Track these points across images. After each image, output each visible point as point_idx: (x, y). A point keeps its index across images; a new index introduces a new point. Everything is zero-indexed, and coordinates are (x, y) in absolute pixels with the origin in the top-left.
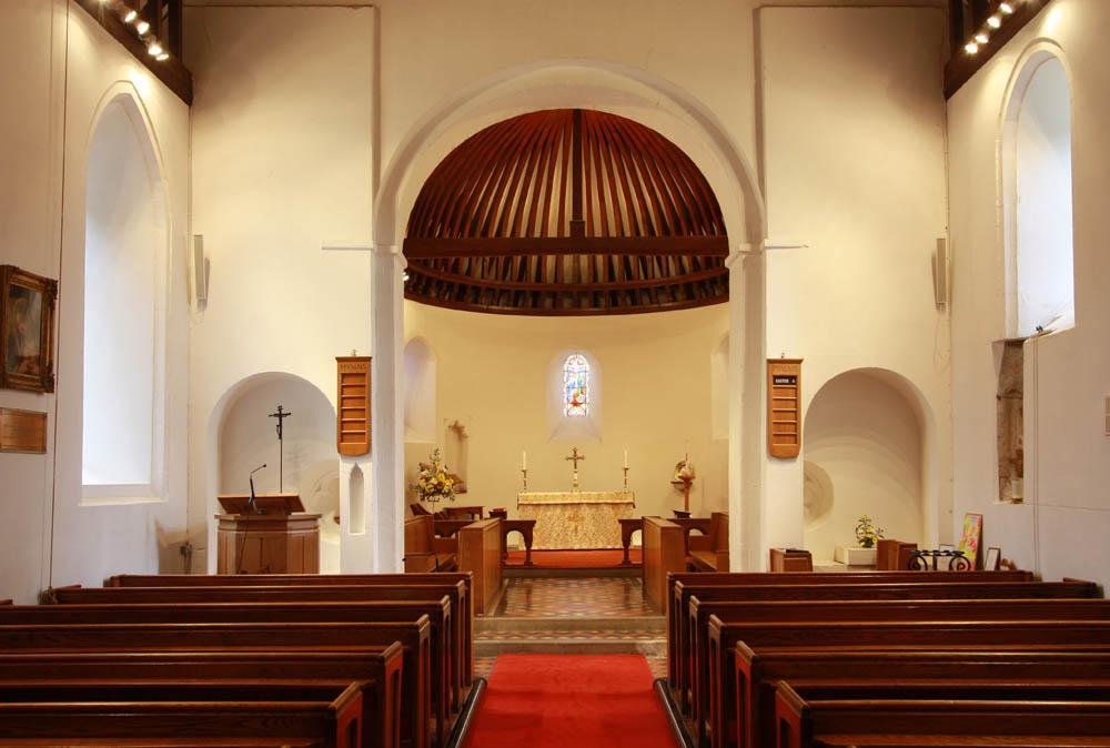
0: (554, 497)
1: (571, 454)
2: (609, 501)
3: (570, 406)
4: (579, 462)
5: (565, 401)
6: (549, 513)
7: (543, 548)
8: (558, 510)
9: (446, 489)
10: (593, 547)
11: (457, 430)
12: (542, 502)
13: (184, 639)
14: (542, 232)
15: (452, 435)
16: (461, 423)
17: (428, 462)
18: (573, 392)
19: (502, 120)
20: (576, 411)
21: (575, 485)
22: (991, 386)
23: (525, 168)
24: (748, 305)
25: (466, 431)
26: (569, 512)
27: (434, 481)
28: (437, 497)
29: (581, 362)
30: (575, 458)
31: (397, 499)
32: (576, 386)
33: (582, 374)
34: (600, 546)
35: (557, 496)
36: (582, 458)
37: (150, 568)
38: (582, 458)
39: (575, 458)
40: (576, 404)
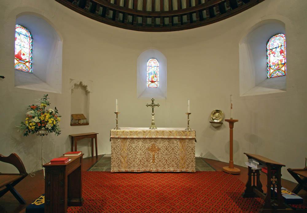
0: (136, 133)
1: (155, 103)
2: (179, 137)
3: (150, 82)
4: (156, 108)
5: (148, 80)
6: (134, 146)
7: (129, 170)
8: (141, 143)
10: (166, 170)
12: (128, 137)
15: (80, 90)
16: (84, 84)
18: (151, 76)
20: (153, 85)
21: (153, 124)
22: (187, 122)
25: (89, 89)
26: (148, 145)
27: (36, 120)
29: (155, 62)
30: (153, 105)
31: (178, 128)
32: (153, 73)
33: (156, 67)
34: (172, 169)
36: (158, 105)
37: (230, 119)
38: (158, 105)
39: (153, 105)
40: (152, 82)
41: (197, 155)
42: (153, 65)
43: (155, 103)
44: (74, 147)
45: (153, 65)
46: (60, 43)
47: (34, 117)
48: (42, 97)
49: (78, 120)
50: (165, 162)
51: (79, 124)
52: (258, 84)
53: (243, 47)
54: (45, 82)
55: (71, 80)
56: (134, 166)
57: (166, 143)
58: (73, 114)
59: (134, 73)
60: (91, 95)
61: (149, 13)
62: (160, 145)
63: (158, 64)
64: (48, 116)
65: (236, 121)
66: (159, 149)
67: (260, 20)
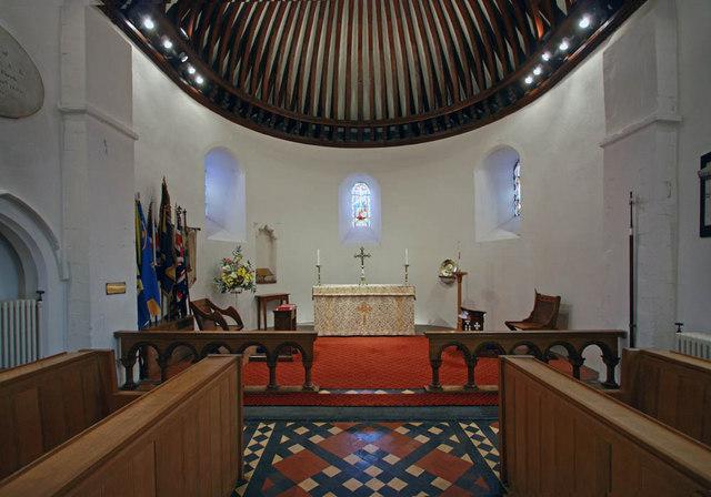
1: (359, 253)
4: (366, 259)
8: (348, 302)
9: (246, 282)
10: (378, 333)
11: (268, 232)
13: (416, 51)
14: (127, 379)
15: (264, 237)
16: (270, 228)
17: (232, 258)
18: (358, 210)
19: (508, 117)
20: (361, 224)
21: (362, 279)
23: (600, 29)
24: (375, 107)
25: (275, 234)
26: (358, 303)
27: (234, 275)
28: (237, 289)
30: (362, 256)
34: (386, 333)
35: (346, 288)
39: (362, 256)
40: (360, 218)
41: (417, 322)
42: (361, 193)
43: (365, 253)
44: (262, 312)
45: (361, 193)
46: (242, 177)
47: (230, 273)
48: (234, 249)
49: (265, 277)
50: (378, 323)
51: (265, 282)
52: (502, 225)
53: (480, 178)
54: (223, 227)
55: (256, 224)
56: (342, 329)
57: (380, 301)
58: (698, 231)
59: (334, 204)
60: (278, 242)
61: (355, 122)
62: (372, 303)
63: (368, 191)
64: (244, 271)
65: (466, 274)
66: (370, 309)
67: (498, 144)
